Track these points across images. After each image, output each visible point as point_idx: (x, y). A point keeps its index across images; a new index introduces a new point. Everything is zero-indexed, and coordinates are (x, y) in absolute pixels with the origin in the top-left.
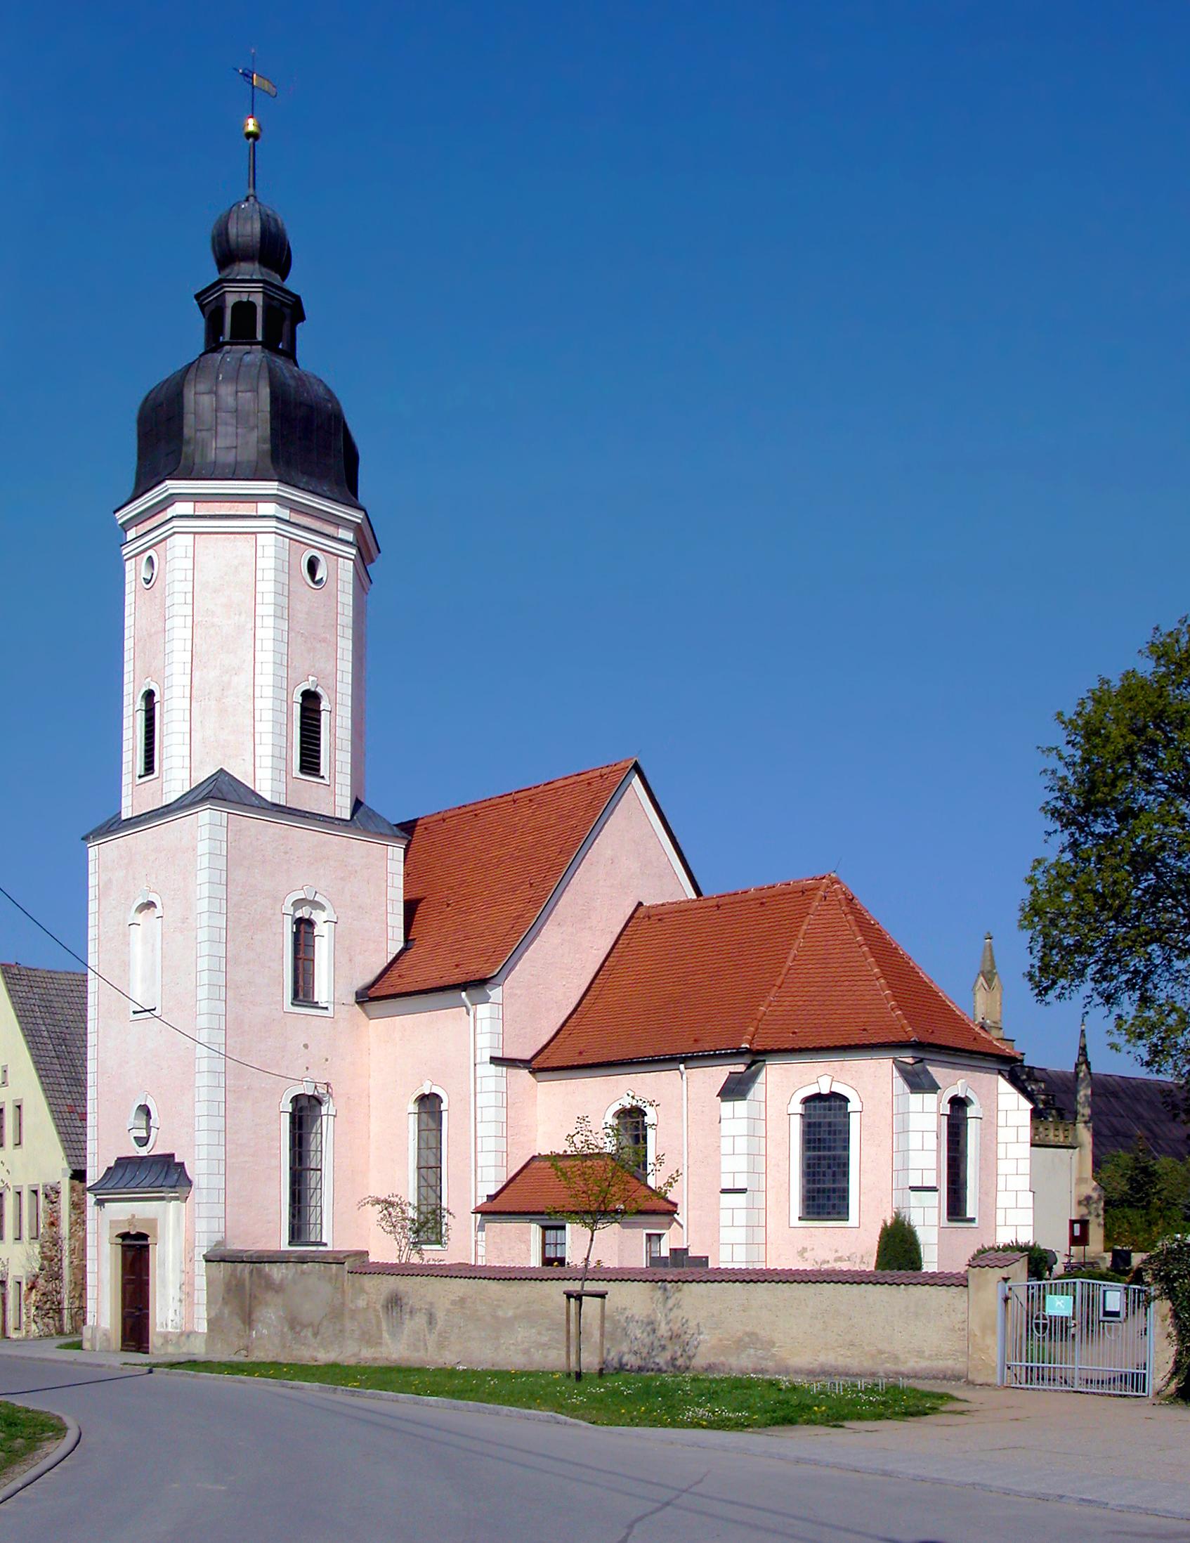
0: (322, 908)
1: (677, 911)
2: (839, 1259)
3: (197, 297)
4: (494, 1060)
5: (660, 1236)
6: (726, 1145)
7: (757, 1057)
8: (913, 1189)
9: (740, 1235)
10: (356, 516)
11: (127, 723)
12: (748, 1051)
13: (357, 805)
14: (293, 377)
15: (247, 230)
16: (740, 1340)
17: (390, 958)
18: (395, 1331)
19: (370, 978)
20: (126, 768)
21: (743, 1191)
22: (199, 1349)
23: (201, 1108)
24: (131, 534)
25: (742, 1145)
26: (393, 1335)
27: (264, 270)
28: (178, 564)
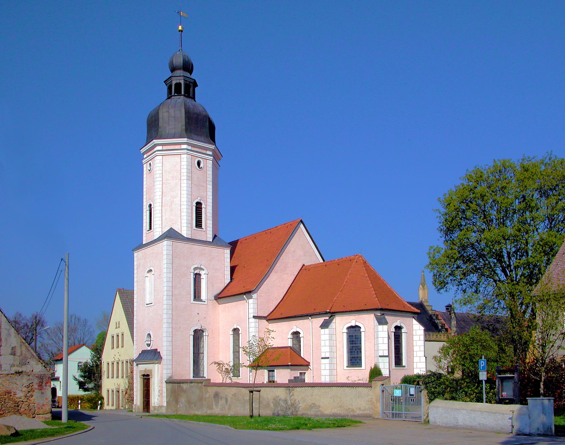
0: (203, 270)
1: (316, 266)
2: (359, 380)
3: (165, 82)
4: (254, 317)
5: (305, 373)
6: (323, 343)
7: (332, 314)
8: (380, 356)
9: (327, 373)
10: (213, 147)
11: (144, 214)
12: (329, 312)
13: (215, 237)
14: (192, 105)
15: (179, 61)
16: (311, 405)
17: (226, 285)
18: (217, 405)
19: (219, 291)
20: (144, 228)
21: (328, 358)
22: (163, 411)
23: (164, 334)
24: (145, 156)
25: (327, 343)
26: (216, 405)
27: (185, 72)
28: (157, 165)
